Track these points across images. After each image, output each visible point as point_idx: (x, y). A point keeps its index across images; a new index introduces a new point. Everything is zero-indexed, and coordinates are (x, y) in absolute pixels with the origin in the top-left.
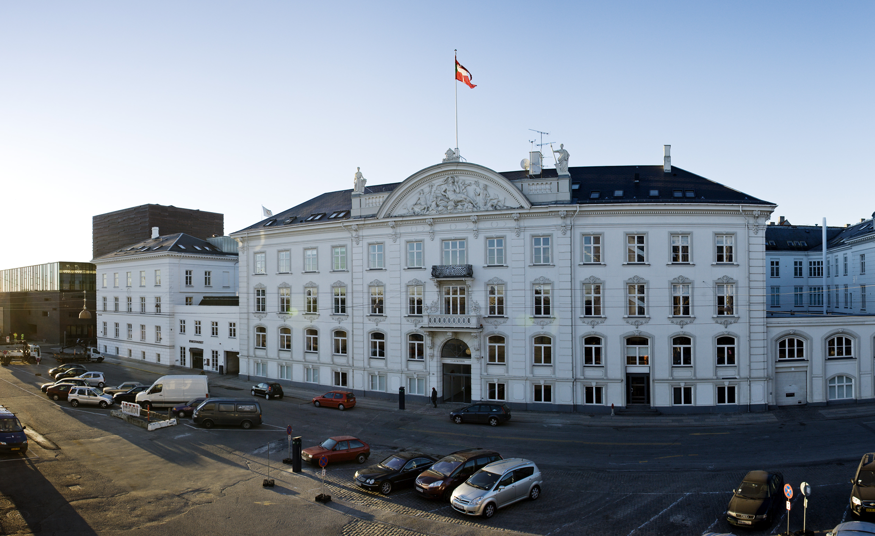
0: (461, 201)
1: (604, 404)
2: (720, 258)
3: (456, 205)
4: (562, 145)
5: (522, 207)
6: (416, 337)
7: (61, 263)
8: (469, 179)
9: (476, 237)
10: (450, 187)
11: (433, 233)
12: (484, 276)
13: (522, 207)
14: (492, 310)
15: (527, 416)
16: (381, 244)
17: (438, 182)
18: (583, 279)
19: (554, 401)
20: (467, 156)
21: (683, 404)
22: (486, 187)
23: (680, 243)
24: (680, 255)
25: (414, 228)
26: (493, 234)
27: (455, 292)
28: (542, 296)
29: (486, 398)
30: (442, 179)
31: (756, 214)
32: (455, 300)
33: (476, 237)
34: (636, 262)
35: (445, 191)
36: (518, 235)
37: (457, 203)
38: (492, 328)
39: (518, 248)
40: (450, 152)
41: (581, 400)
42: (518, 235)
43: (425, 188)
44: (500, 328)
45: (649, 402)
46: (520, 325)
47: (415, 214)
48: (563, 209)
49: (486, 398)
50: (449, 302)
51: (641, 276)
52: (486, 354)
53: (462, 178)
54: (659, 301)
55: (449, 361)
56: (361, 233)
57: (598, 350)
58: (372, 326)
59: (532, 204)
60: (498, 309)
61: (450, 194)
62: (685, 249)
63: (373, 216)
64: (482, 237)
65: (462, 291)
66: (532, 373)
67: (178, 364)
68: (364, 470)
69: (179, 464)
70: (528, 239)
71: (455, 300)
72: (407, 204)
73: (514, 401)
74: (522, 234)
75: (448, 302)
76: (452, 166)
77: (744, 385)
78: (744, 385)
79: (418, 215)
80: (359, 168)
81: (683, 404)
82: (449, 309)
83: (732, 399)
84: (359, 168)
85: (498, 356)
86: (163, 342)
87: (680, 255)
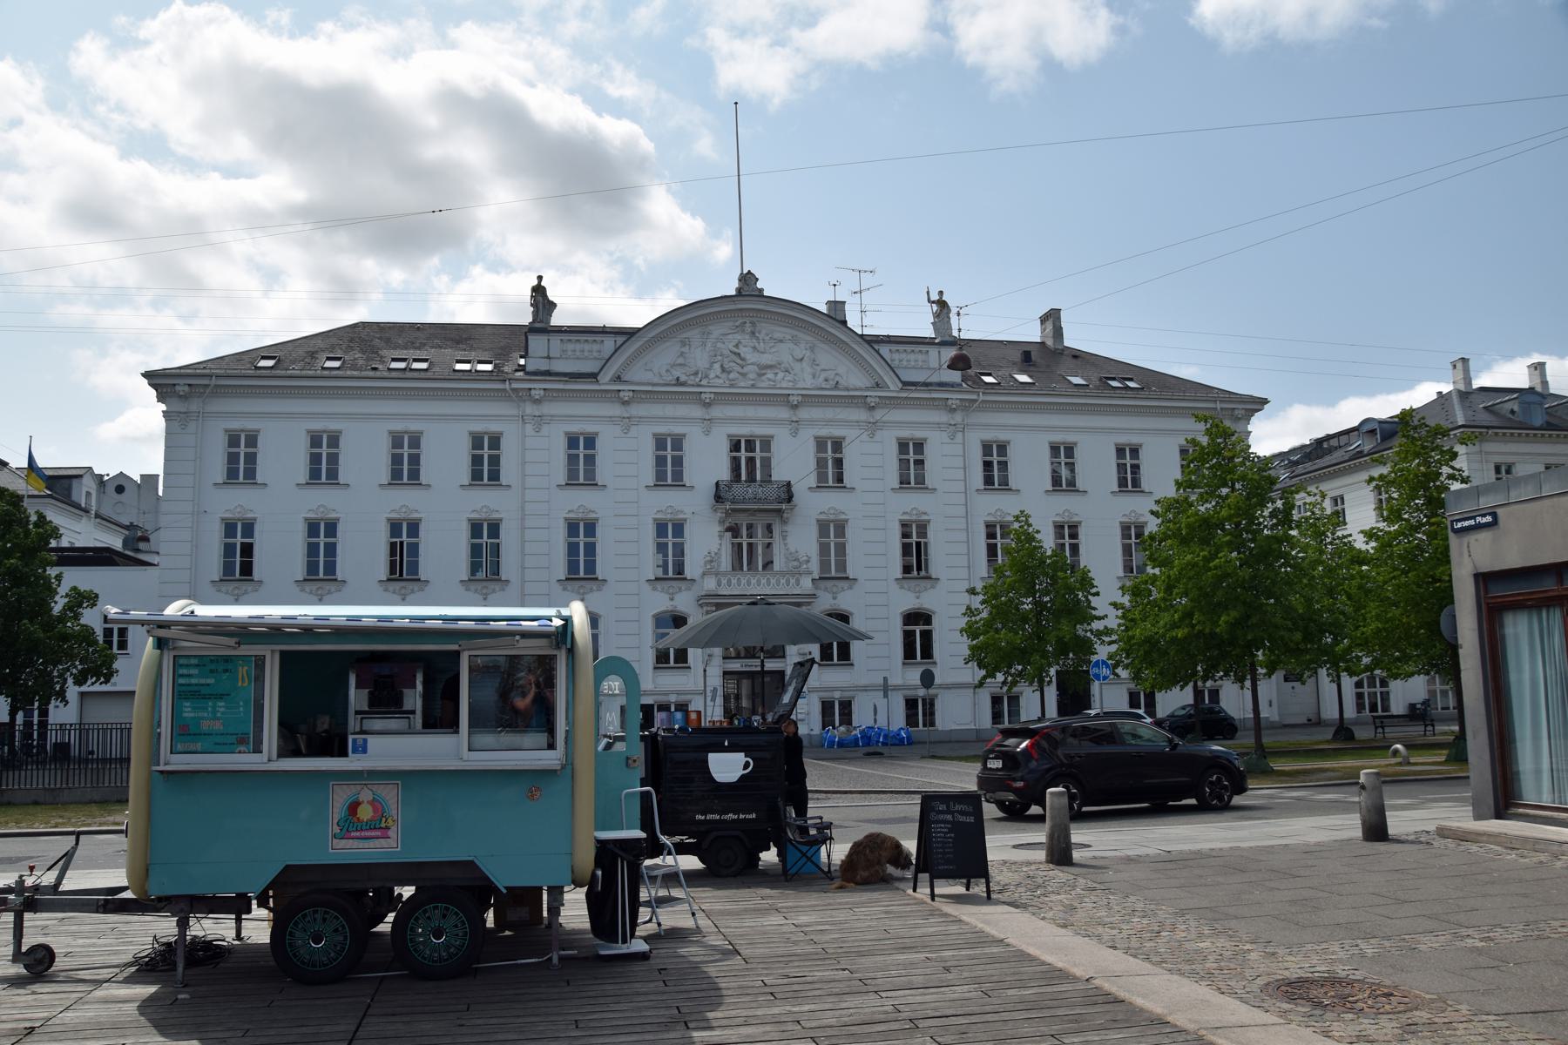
0: (771, 367)
4: (941, 293)
6: (917, 618)
9: (795, 433)
12: (813, 504)
15: (1334, 442)
20: (771, 286)
24: (405, 466)
25: (670, 410)
26: (824, 432)
31: (626, 396)
32: (751, 461)
33: (795, 433)
35: (737, 346)
37: (764, 368)
39: (871, 460)
46: (876, 600)
47: (678, 382)
48: (954, 397)
60: (834, 570)
63: (593, 376)
66: (615, 878)
67: (660, 575)
68: (781, 804)
71: (751, 461)
74: (959, 435)
79: (683, 384)
80: (540, 278)
84: (540, 278)
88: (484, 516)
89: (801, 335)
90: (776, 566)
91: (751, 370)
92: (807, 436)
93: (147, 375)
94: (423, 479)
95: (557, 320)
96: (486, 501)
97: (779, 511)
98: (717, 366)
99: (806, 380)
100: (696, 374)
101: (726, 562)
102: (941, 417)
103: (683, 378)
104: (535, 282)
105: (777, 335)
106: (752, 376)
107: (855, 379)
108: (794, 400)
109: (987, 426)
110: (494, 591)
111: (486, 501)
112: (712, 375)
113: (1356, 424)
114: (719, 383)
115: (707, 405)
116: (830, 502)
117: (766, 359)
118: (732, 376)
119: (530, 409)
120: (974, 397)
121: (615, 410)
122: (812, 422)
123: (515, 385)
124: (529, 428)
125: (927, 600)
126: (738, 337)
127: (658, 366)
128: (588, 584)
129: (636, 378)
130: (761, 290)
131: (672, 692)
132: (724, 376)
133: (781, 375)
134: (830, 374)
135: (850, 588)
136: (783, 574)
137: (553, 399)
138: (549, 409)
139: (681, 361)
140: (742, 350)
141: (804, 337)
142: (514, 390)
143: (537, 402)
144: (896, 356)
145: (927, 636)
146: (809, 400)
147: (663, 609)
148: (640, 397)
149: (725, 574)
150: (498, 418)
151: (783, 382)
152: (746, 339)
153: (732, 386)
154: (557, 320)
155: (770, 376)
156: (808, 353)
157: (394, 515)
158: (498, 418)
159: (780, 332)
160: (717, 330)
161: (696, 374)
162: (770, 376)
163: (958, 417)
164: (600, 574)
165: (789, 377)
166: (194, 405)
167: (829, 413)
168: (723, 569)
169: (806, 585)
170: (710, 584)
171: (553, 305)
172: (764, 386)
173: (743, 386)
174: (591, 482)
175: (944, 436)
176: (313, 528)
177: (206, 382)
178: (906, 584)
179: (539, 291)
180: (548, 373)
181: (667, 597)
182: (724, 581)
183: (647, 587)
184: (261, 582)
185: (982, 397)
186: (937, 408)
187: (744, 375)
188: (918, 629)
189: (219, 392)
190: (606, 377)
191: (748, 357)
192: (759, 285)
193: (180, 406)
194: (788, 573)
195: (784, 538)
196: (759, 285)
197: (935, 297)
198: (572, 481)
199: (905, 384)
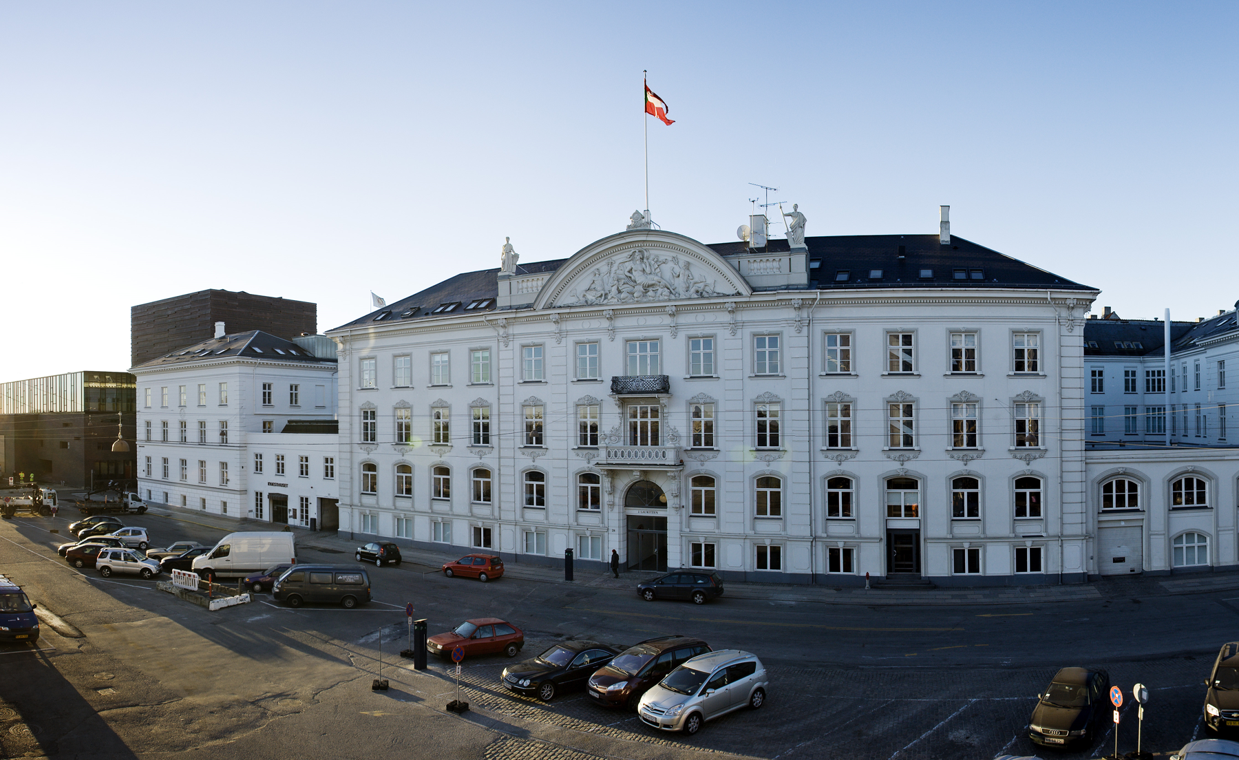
0: (652, 285)
1: (855, 572)
3: (646, 291)
4: (796, 206)
5: (739, 294)
6: (589, 477)
8: (664, 254)
9: (675, 336)
10: (637, 266)
11: (613, 331)
12: (685, 391)
13: (739, 294)
14: (697, 439)
15: (746, 590)
16: (539, 346)
17: (620, 258)
18: (825, 396)
19: (785, 568)
20: (662, 221)
21: (967, 573)
22: (688, 266)
23: (962, 345)
24: (963, 361)
25: (587, 324)
26: (698, 332)
27: (644, 415)
29: (689, 564)
30: (626, 254)
32: (644, 425)
33: (675, 336)
35: (630, 271)
36: (734, 333)
37: (646, 288)
38: (697, 465)
39: (734, 352)
40: (637, 216)
42: (734, 333)
43: (602, 266)
44: (709, 466)
45: (919, 570)
46: (736, 461)
47: (587, 304)
48: (797, 297)
49: (689, 564)
50: (635, 429)
51: (908, 391)
52: (688, 502)
53: (654, 252)
54: (933, 427)
55: (636, 512)
56: (511, 330)
57: (847, 497)
58: (527, 462)
59: (754, 290)
60: (705, 438)
61: (637, 276)
62: (970, 353)
63: (529, 306)
64: (682, 336)
65: (655, 413)
67: (252, 516)
68: (515, 667)
70: (747, 338)
71: (644, 425)
72: (577, 290)
73: (727, 569)
74: (739, 332)
75: (634, 428)
76: (640, 236)
77: (1054, 547)
78: (1054, 547)
79: (591, 305)
80: (508, 239)
81: (967, 573)
82: (636, 438)
84: (508, 239)
85: (705, 505)
86: (230, 486)
87: (963, 361)
113: (1210, 314)
137: (743, 309)
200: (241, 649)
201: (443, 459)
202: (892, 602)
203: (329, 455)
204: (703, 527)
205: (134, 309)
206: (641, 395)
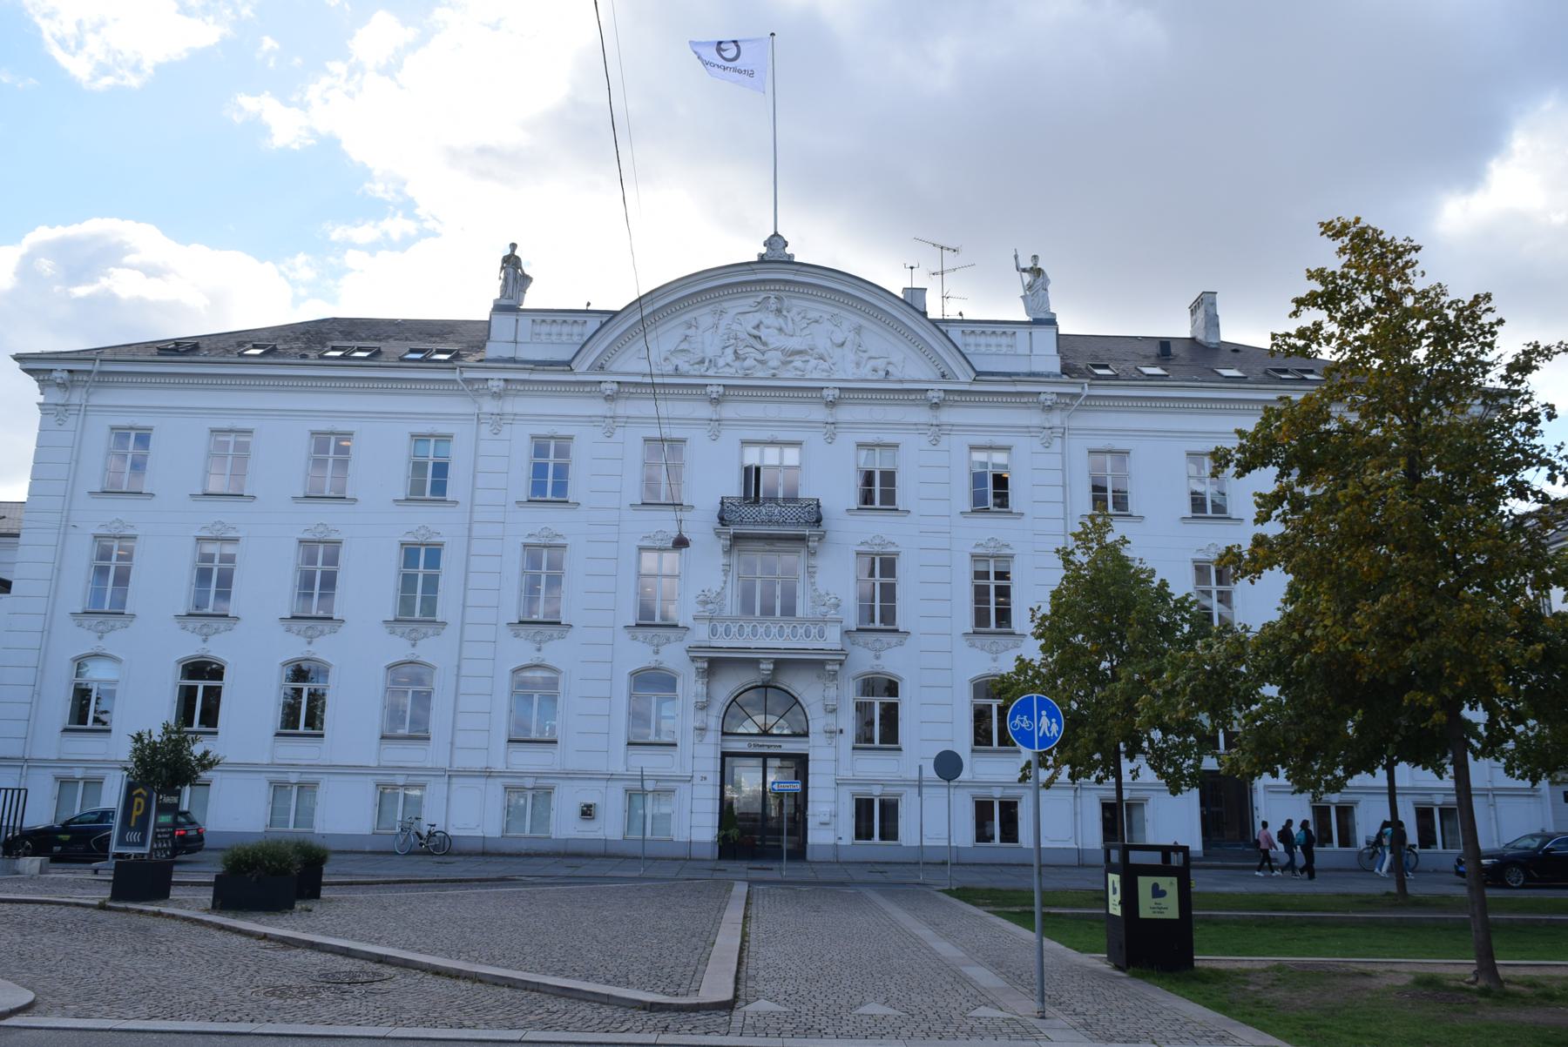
0: (800, 352)
2: (867, 498)
7: (446, 465)
9: (831, 439)
12: (854, 531)
14: (867, 612)
20: (803, 250)
23: (878, 463)
28: (216, 567)
30: (751, 301)
34: (428, 495)
35: (757, 327)
38: (868, 659)
41: (965, 835)
43: (704, 316)
44: (892, 660)
48: (1048, 391)
52: (848, 721)
60: (881, 612)
62: (889, 478)
63: (567, 365)
69: (1134, 976)
80: (514, 246)
83: (890, 832)
84: (514, 246)
85: (881, 723)
88: (420, 539)
89: (844, 313)
90: (799, 613)
91: (774, 359)
92: (632, 441)
93: (18, 358)
94: (900, 503)
95: (533, 299)
96: (426, 521)
97: (802, 539)
98: (730, 351)
99: (848, 369)
100: (702, 362)
101: (731, 605)
102: (1034, 418)
103: (684, 367)
104: (508, 252)
105: (813, 315)
106: (774, 363)
107: (913, 369)
108: (829, 395)
109: (1095, 431)
110: (425, 635)
111: (426, 521)
112: (721, 362)
114: (728, 371)
115: (716, 401)
116: (877, 529)
117: (794, 343)
118: (748, 363)
119: (489, 405)
120: (1077, 390)
121: (598, 408)
122: (854, 425)
123: (467, 375)
124: (485, 430)
125: (322, 648)
126: (758, 316)
127: (661, 350)
128: (885, 638)
129: (614, 368)
130: (792, 256)
131: (876, 782)
132: (737, 364)
133: (813, 362)
134: (881, 364)
135: (901, 644)
136: (803, 621)
138: (511, 406)
139: (684, 346)
140: (763, 333)
141: (850, 319)
142: (466, 381)
143: (497, 395)
144: (971, 340)
145: (213, 696)
146: (848, 394)
147: (985, 672)
148: (627, 389)
149: (734, 620)
150: (448, 417)
151: (813, 372)
152: (770, 319)
153: (746, 377)
154: (533, 299)
155: (798, 363)
156: (851, 336)
157: (1199, 556)
158: (448, 417)
159: (817, 309)
160: (734, 307)
161: (702, 362)
162: (798, 363)
163: (1056, 419)
164: (900, 624)
165: (825, 366)
166: (77, 397)
167: (772, 410)
168: (727, 612)
169: (833, 638)
170: (701, 634)
171: (527, 280)
172: (788, 377)
173: (760, 376)
174: (560, 496)
175: (1036, 444)
176: (410, 553)
177: (88, 367)
178: (979, 640)
179: (511, 262)
180: (513, 360)
181: (304, 640)
182: (721, 629)
183: (624, 636)
184: (134, 616)
185: (1087, 391)
186: (1026, 406)
187: (762, 362)
188: (201, 685)
189: (105, 379)
190: (582, 366)
191: (770, 340)
192: (788, 250)
193: (58, 396)
194: (815, 622)
195: (811, 574)
196: (788, 250)
197: (1027, 263)
198: (415, 495)
199: (979, 374)
200: (57, 859)
201: (541, 655)
202: (1245, 966)
203: (600, 812)
204: (878, 771)
205: (632, 674)
206: (765, 521)
